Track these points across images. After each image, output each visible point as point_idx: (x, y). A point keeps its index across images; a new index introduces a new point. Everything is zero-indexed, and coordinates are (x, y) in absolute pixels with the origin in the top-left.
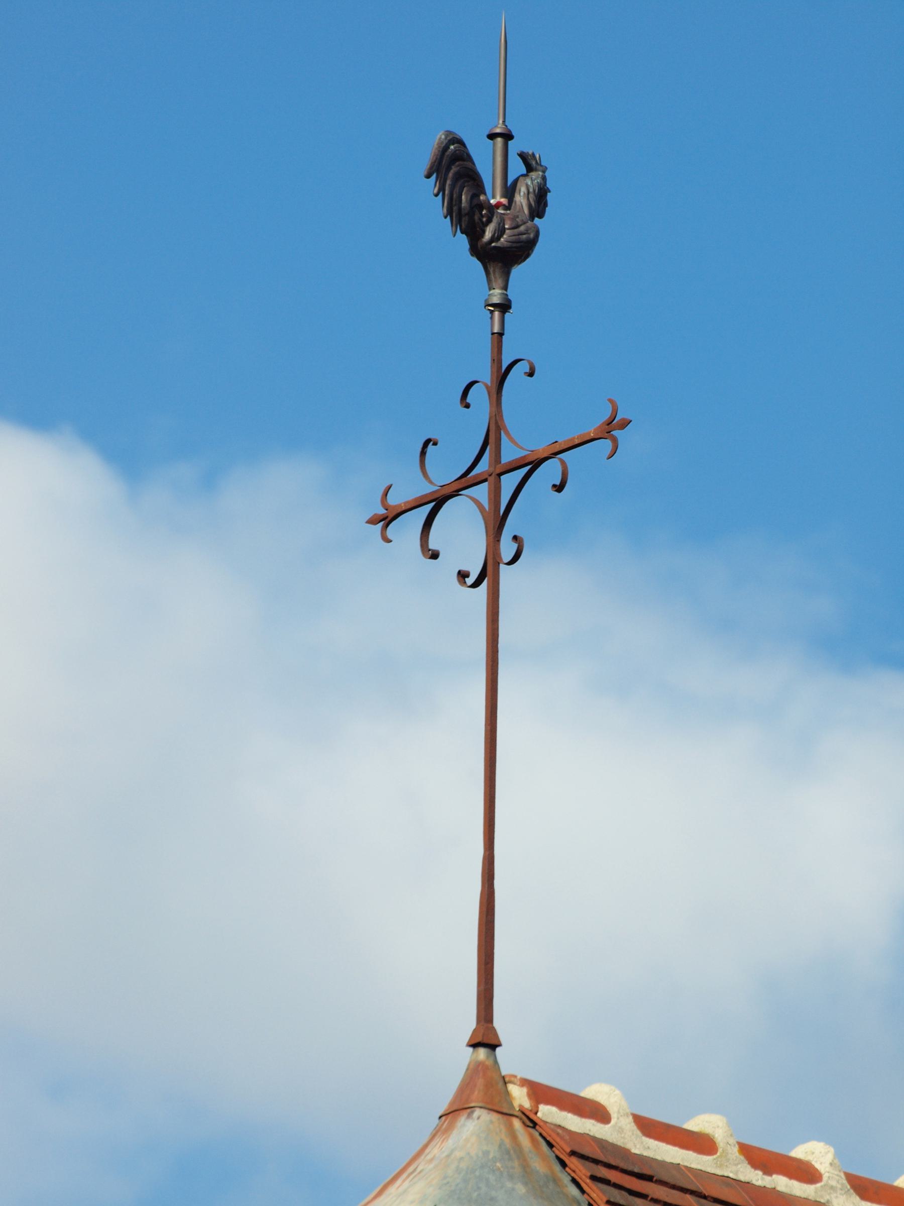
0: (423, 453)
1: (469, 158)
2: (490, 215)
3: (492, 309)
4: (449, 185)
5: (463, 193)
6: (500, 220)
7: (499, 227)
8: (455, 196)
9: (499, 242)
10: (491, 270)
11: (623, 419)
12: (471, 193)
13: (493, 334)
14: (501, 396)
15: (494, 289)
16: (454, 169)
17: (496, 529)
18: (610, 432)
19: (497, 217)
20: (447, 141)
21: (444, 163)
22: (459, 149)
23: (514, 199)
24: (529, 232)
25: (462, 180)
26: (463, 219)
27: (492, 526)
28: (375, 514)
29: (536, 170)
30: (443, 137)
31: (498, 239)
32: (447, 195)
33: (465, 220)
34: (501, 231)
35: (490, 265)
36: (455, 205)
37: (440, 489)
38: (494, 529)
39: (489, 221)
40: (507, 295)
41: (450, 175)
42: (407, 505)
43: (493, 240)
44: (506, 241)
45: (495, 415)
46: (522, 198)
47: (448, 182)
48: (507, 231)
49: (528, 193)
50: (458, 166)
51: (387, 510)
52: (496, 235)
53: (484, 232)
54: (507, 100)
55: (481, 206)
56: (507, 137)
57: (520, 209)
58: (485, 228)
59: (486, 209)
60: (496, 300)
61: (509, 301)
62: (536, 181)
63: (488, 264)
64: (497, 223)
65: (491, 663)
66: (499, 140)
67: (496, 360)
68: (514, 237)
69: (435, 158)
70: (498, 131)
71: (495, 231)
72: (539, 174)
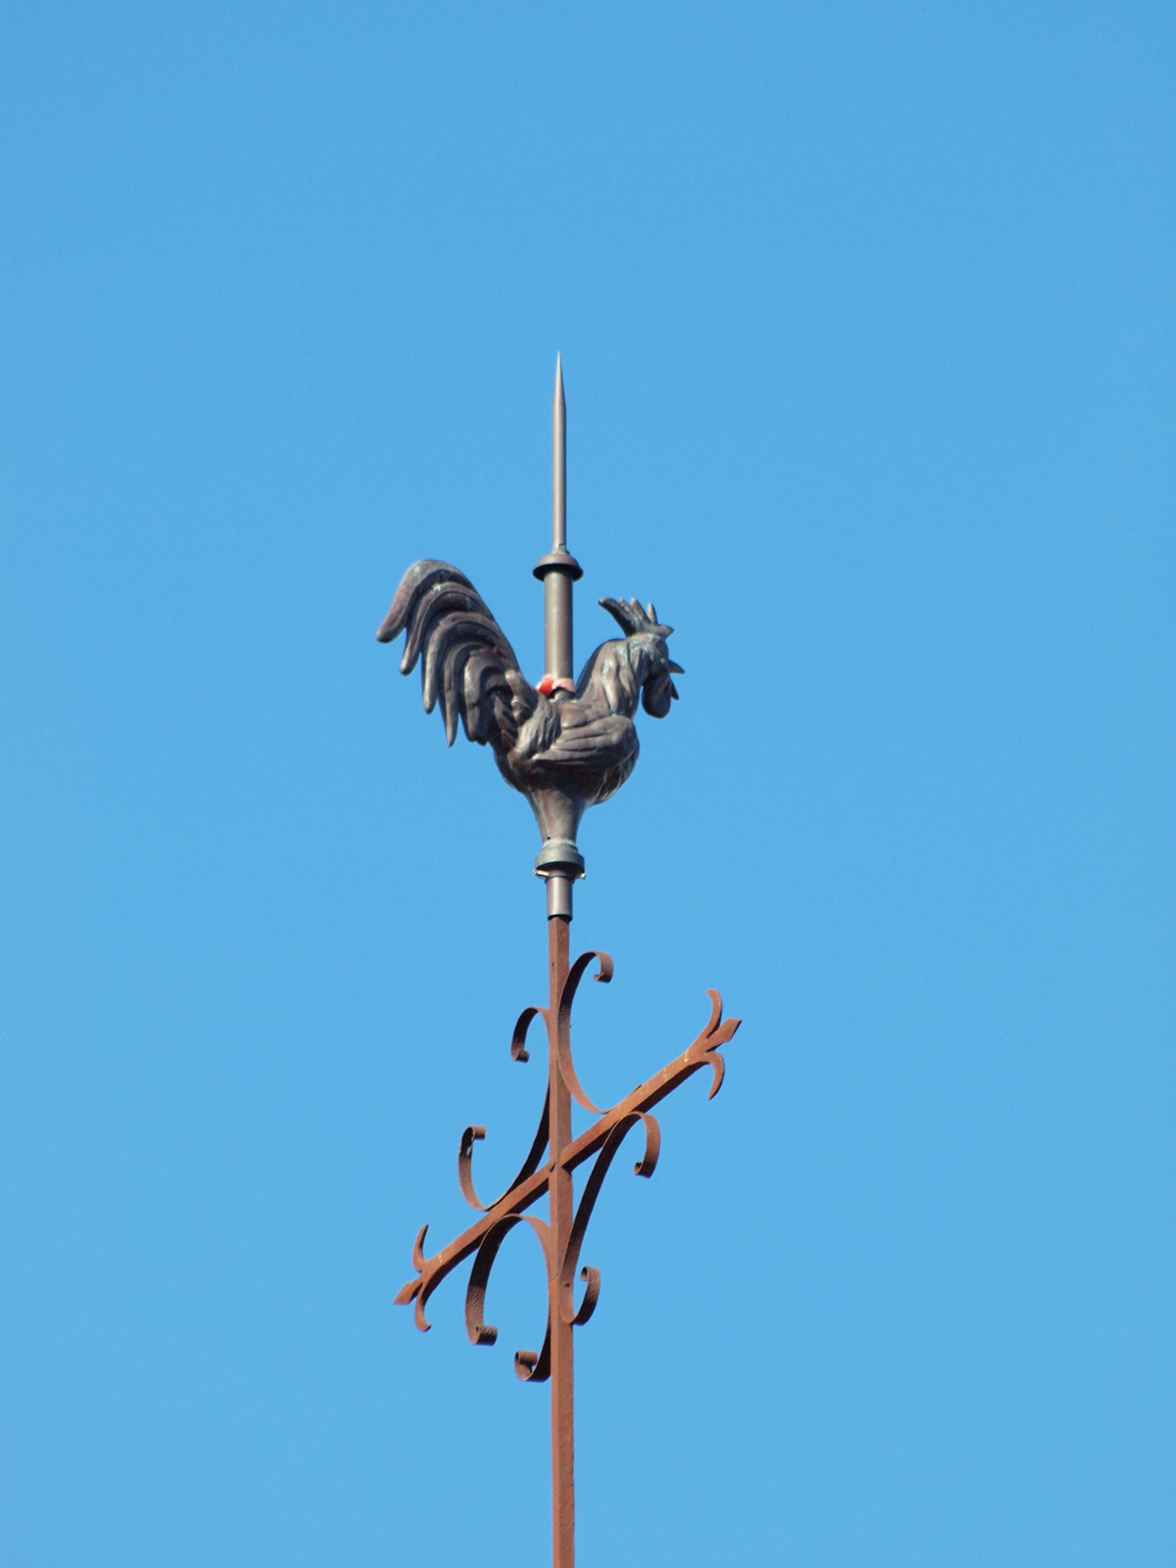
0: (465, 1155)
1: (477, 605)
2: (526, 705)
3: (546, 874)
4: (434, 653)
5: (466, 669)
6: (548, 713)
7: (545, 727)
8: (447, 674)
9: (547, 752)
10: (541, 805)
11: (729, 1021)
12: (482, 668)
13: (551, 918)
14: (568, 1026)
15: (549, 838)
16: (444, 625)
17: (562, 1266)
18: (714, 1048)
19: (543, 708)
20: (424, 577)
21: (419, 615)
22: (454, 590)
23: (591, 681)
24: (608, 731)
25: (463, 645)
26: (470, 714)
27: (556, 1260)
28: (407, 1285)
29: (642, 630)
30: (417, 569)
31: (546, 746)
32: (431, 670)
33: (473, 716)
34: (553, 732)
35: (536, 795)
36: (450, 689)
37: (488, 1215)
38: (559, 1266)
39: (526, 715)
40: (575, 848)
41: (436, 636)
42: (445, 1255)
43: (532, 751)
44: (562, 750)
45: (557, 1061)
46: (604, 677)
47: (432, 649)
48: (565, 733)
49: (618, 668)
50: (453, 620)
51: (420, 1272)
52: (540, 740)
53: (516, 735)
54: (568, 503)
55: (506, 692)
56: (571, 571)
57: (598, 696)
58: (519, 729)
59: (517, 694)
60: (553, 856)
61: (581, 859)
62: (637, 648)
63: (533, 794)
64: (542, 718)
65: (558, 1507)
66: (554, 578)
67: (556, 966)
68: (575, 742)
69: (398, 607)
70: (551, 560)
71: (537, 732)
72: (648, 637)
